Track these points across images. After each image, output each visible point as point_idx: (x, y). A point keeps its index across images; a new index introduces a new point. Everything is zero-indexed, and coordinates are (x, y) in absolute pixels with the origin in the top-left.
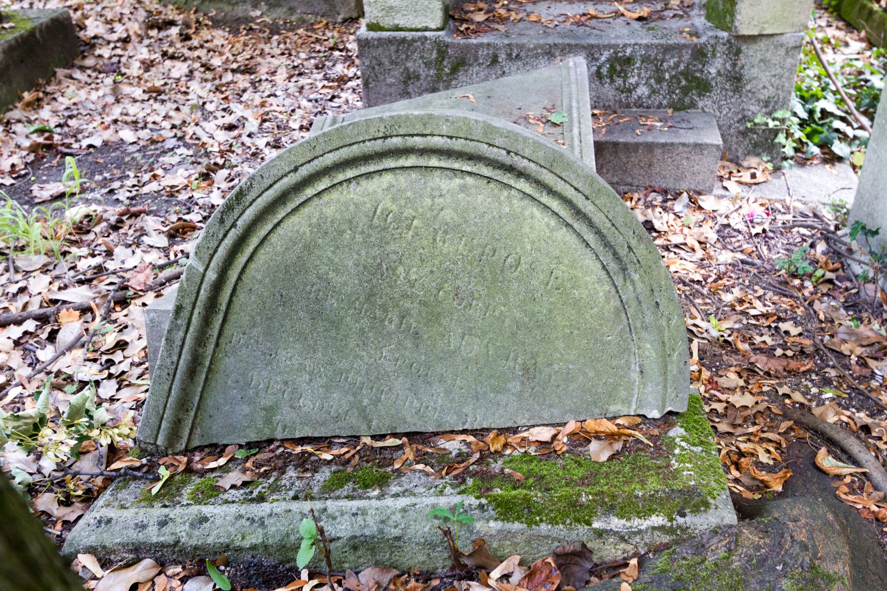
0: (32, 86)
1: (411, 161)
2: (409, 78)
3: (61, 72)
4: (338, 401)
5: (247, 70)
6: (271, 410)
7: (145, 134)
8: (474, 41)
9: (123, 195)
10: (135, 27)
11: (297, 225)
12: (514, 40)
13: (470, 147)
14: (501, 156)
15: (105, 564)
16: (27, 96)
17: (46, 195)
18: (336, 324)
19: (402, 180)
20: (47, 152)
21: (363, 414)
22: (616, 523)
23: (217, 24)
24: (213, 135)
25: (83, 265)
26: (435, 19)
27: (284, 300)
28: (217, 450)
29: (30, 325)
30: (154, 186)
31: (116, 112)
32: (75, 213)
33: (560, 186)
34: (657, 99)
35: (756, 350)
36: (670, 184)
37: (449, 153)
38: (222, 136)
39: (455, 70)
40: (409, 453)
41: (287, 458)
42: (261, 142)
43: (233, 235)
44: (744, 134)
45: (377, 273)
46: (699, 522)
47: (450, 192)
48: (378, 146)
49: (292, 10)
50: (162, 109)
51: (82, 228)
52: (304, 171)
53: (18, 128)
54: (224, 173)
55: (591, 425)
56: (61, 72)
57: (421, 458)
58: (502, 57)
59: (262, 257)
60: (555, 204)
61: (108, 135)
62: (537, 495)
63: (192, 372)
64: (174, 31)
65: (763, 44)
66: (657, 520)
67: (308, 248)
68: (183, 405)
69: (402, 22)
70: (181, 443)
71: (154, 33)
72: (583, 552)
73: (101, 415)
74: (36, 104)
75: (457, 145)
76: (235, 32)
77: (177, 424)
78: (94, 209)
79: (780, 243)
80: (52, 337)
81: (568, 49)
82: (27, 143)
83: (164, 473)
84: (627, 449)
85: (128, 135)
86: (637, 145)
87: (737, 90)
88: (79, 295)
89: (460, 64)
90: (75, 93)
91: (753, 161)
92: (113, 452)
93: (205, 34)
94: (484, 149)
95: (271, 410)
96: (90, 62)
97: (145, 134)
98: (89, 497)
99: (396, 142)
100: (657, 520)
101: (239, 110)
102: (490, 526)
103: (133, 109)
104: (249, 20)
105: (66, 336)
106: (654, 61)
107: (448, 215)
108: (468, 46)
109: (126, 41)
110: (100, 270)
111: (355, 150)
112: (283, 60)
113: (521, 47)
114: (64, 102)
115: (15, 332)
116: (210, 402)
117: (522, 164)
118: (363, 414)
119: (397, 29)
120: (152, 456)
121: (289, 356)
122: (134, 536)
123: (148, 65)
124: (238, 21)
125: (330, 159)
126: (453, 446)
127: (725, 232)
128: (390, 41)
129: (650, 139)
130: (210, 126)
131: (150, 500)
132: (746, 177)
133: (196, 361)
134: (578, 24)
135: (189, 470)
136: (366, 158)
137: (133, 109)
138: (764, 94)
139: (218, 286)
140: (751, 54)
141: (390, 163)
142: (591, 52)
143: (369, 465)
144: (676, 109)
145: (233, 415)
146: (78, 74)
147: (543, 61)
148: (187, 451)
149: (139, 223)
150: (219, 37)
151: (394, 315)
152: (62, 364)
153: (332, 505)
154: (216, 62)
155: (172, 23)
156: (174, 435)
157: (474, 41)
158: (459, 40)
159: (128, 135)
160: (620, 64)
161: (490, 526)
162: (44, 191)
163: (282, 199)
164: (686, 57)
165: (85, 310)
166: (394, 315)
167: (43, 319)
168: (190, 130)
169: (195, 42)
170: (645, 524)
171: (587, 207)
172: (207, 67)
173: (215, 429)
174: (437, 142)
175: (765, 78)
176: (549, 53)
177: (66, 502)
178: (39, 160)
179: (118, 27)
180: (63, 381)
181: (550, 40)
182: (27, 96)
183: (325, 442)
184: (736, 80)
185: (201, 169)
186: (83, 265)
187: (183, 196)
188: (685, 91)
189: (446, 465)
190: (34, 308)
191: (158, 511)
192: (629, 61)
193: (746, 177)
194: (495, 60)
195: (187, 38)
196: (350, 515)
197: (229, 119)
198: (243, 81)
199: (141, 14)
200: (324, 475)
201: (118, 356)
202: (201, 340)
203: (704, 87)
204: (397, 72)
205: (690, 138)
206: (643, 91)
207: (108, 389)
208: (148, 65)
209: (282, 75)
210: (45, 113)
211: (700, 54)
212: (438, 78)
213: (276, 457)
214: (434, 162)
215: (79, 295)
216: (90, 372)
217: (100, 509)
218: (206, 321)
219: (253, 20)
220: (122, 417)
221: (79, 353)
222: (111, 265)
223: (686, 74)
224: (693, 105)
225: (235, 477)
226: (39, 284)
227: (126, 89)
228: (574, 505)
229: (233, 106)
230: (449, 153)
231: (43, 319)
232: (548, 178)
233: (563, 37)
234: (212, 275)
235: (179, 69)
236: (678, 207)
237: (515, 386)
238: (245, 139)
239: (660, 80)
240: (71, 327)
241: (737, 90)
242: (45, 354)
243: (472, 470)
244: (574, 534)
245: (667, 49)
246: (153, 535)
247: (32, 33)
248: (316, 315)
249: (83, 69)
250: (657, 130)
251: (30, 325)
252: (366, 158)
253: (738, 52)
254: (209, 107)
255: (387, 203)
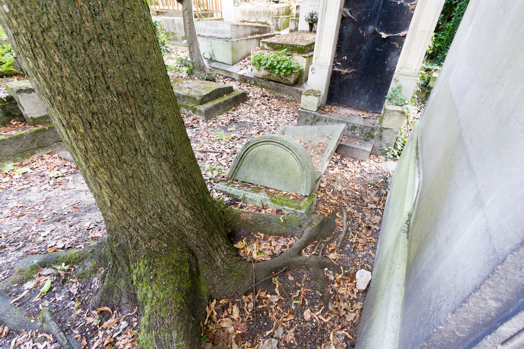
0: (235, 106)
1: (274, 143)
2: (307, 120)
3: (241, 104)
4: (256, 178)
5: (278, 110)
6: (246, 177)
7: (252, 121)
8: (322, 116)
9: (243, 133)
10: (259, 96)
11: (256, 149)
12: (332, 117)
13: (283, 144)
14: (288, 146)
15: (216, 192)
16: (233, 108)
17: (229, 130)
18: (258, 166)
19: (273, 146)
20: (233, 121)
21: (259, 182)
22: (287, 208)
23: (276, 97)
24: (264, 124)
25: (231, 145)
26: (315, 109)
27: (252, 160)
28: (237, 181)
29: (219, 154)
30: (249, 133)
31: (248, 115)
32: (233, 135)
33: (296, 153)
34: (361, 137)
35: (346, 195)
36: (354, 157)
37: (280, 144)
38: (266, 125)
39: (317, 121)
40: (264, 190)
41: (246, 185)
42: (272, 128)
43: (246, 148)
44: (381, 150)
45: (266, 160)
46: (299, 211)
47: (279, 149)
48: (270, 140)
49: (294, 97)
50: (257, 116)
51: (233, 138)
52: (258, 141)
53: (229, 115)
54: (262, 133)
55: (292, 193)
56: (241, 104)
57: (265, 191)
58: (328, 120)
59: (250, 153)
60: (295, 156)
61: (245, 120)
62: (278, 201)
63: (236, 168)
64: (267, 98)
65: (388, 130)
66: (293, 209)
67: (257, 153)
68: (234, 172)
69: (308, 109)
70: (232, 179)
71: (262, 98)
72: (281, 210)
73: (223, 171)
74: (234, 110)
75: (281, 143)
76: (279, 100)
77: (232, 175)
78: (237, 135)
79: (373, 176)
80: (221, 157)
81: (342, 122)
82: (230, 119)
83: (229, 182)
84: (296, 198)
85: (248, 120)
86: (350, 147)
87: (380, 139)
88: (228, 151)
89: (318, 120)
90: (243, 109)
91: (381, 157)
92: (223, 177)
93: (273, 100)
94: (285, 144)
95: (246, 177)
96: (247, 102)
97: (252, 121)
98: (218, 182)
99: (272, 140)
100: (293, 209)
101: (272, 120)
102: (269, 203)
103: (252, 115)
104: (283, 98)
105: (223, 157)
106: (362, 128)
107: (278, 153)
108: (321, 117)
109: (256, 99)
110: (233, 147)
111: (265, 140)
112: (286, 109)
113: (332, 119)
114: (240, 111)
115: (216, 154)
116: (238, 173)
117: (291, 148)
118: (259, 182)
119: (307, 110)
120: (228, 179)
121: (250, 169)
122: (221, 189)
123: (258, 105)
124: (281, 97)
125: (262, 140)
126: (271, 190)
127: (362, 171)
128: (304, 112)
129: (354, 146)
130: (264, 122)
131: (225, 185)
132: (377, 160)
133: (237, 166)
134: (348, 116)
135: (232, 182)
136: (268, 141)
137: (252, 115)
138: (387, 142)
139: (243, 155)
140: (385, 132)
141: (271, 143)
142: (348, 124)
143: (257, 189)
144: (365, 140)
145: (240, 177)
146: (244, 105)
147: (336, 123)
148: (233, 180)
149: (243, 139)
150: (275, 101)
151: (267, 167)
152: (221, 162)
153: (249, 193)
154: (272, 107)
155: (267, 96)
156: (232, 177)
157: (322, 116)
158: (319, 115)
159: (248, 120)
160: (354, 128)
161: (269, 203)
162: (229, 130)
163: (254, 144)
164: (370, 129)
165: (228, 154)
166: (267, 167)
167: (221, 153)
168: (260, 122)
169: (270, 101)
170: (291, 209)
171: (299, 158)
172: (270, 108)
173: (238, 178)
174: (278, 141)
175: (388, 138)
176: (338, 122)
177: (214, 182)
178: (231, 122)
179: (256, 95)
180: (220, 164)
181: (339, 119)
182: (233, 108)
183: (253, 184)
184: (381, 137)
185: (258, 131)
186: (231, 145)
187: (253, 136)
188: (368, 137)
189: (269, 194)
190: (220, 151)
191: (225, 187)
192: (356, 127)
193: (377, 160)
194: (326, 121)
195: (269, 100)
196: (250, 195)
197: (269, 121)
198: (276, 112)
199: (261, 93)
200: (251, 189)
201: (230, 163)
202: (238, 163)
203: (373, 137)
204: (305, 119)
205: (363, 148)
206: (358, 135)
207: (227, 167)
208: (258, 105)
209: (285, 112)
210: (235, 113)
211: (373, 129)
212: (313, 122)
213: (245, 184)
214: (278, 144)
215: (228, 151)
216: (225, 164)
217: (218, 184)
218: (240, 160)
219: (284, 98)
220: (227, 172)
221: (225, 161)
222: (235, 147)
223: (369, 133)
224: (369, 141)
225: (238, 185)
226: (223, 147)
227: (252, 110)
228: (282, 203)
229: (271, 119)
230: (280, 144)
231: (221, 153)
232: (294, 151)
233: (342, 118)
234: (242, 154)
235: (264, 107)
236: (356, 163)
237: (283, 184)
238: (270, 127)
239: (362, 133)
240: (225, 156)
241: (380, 139)
242: (219, 159)
243: (272, 194)
244: (281, 208)
245: (365, 127)
246: (224, 190)
247: (237, 96)
248: (256, 164)
249: (246, 104)
250: (357, 144)
251: (219, 154)
252: (268, 141)
253: (382, 131)
254: (266, 118)
255: (270, 149)
